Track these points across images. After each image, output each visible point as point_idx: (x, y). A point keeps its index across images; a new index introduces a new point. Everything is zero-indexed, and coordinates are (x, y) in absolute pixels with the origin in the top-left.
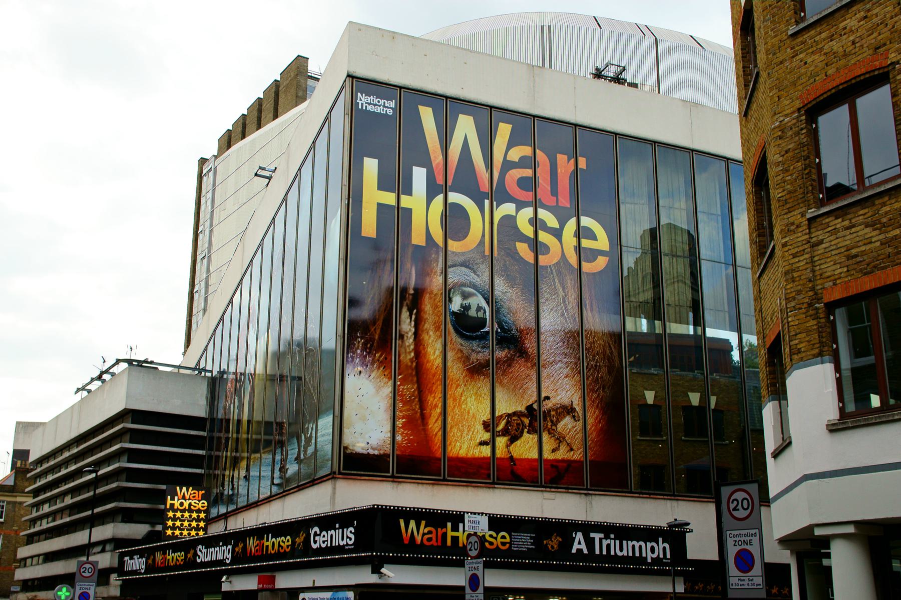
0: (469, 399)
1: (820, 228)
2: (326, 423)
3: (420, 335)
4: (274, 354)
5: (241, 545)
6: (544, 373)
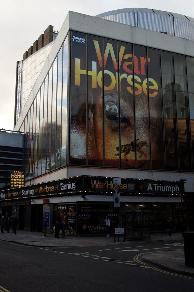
4: (45, 127)
5: (37, 189)
6: (137, 131)
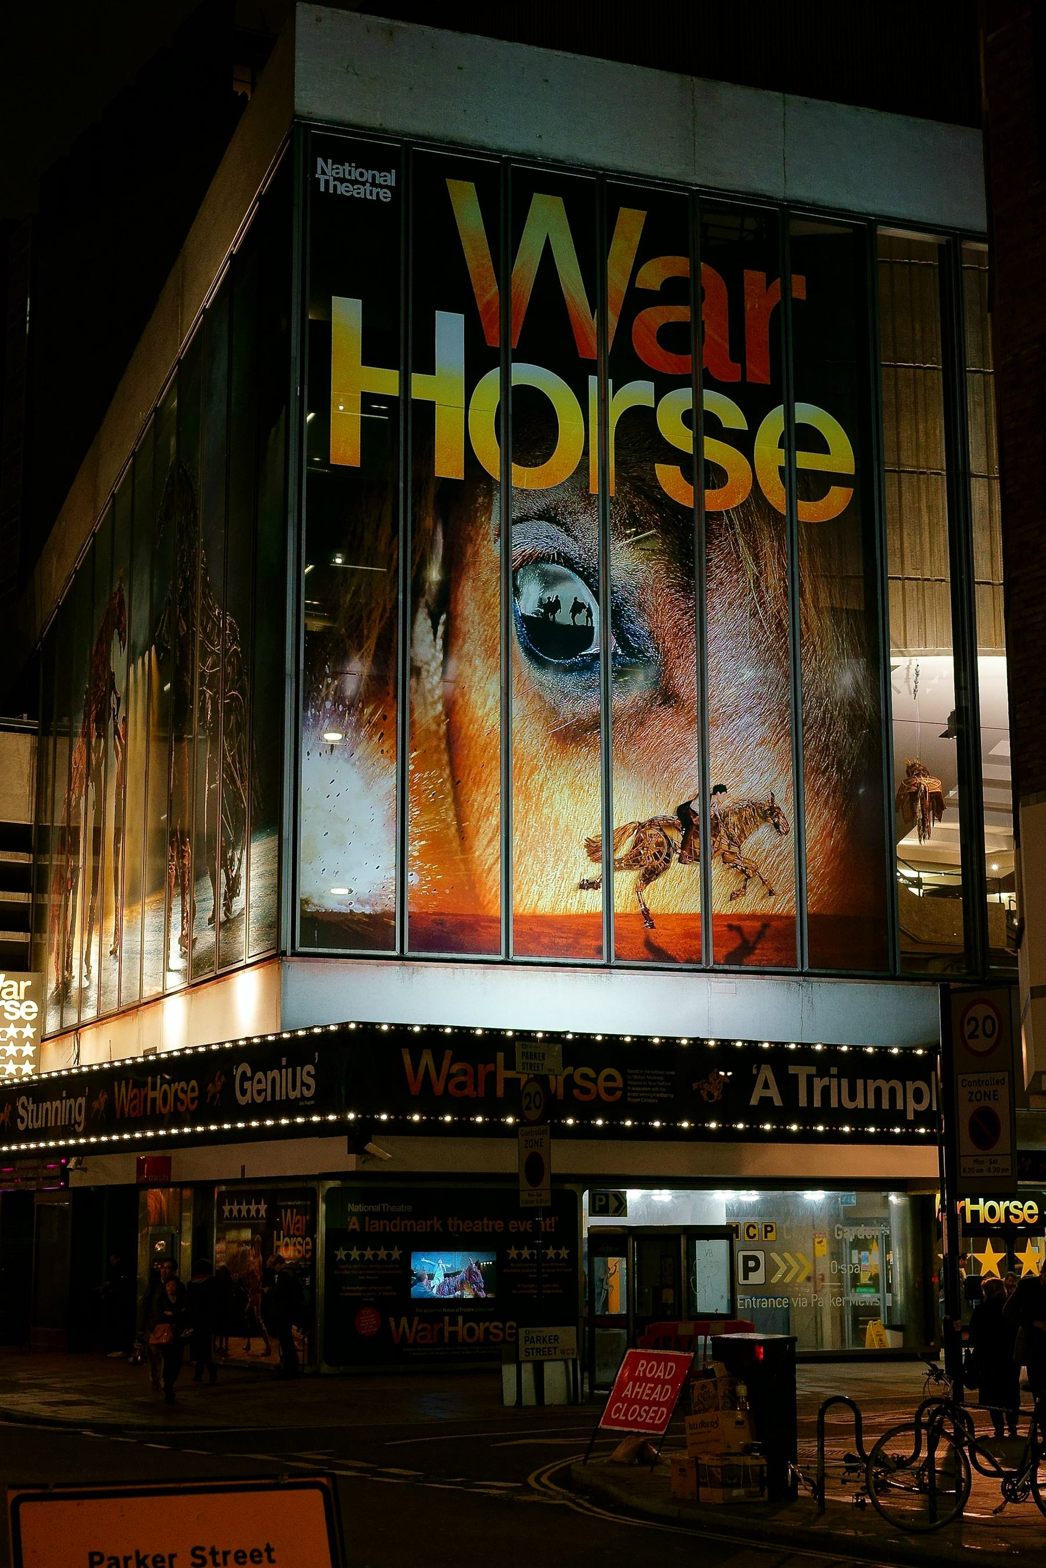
0: (557, 796)
5: (103, 1097)
6: (714, 738)
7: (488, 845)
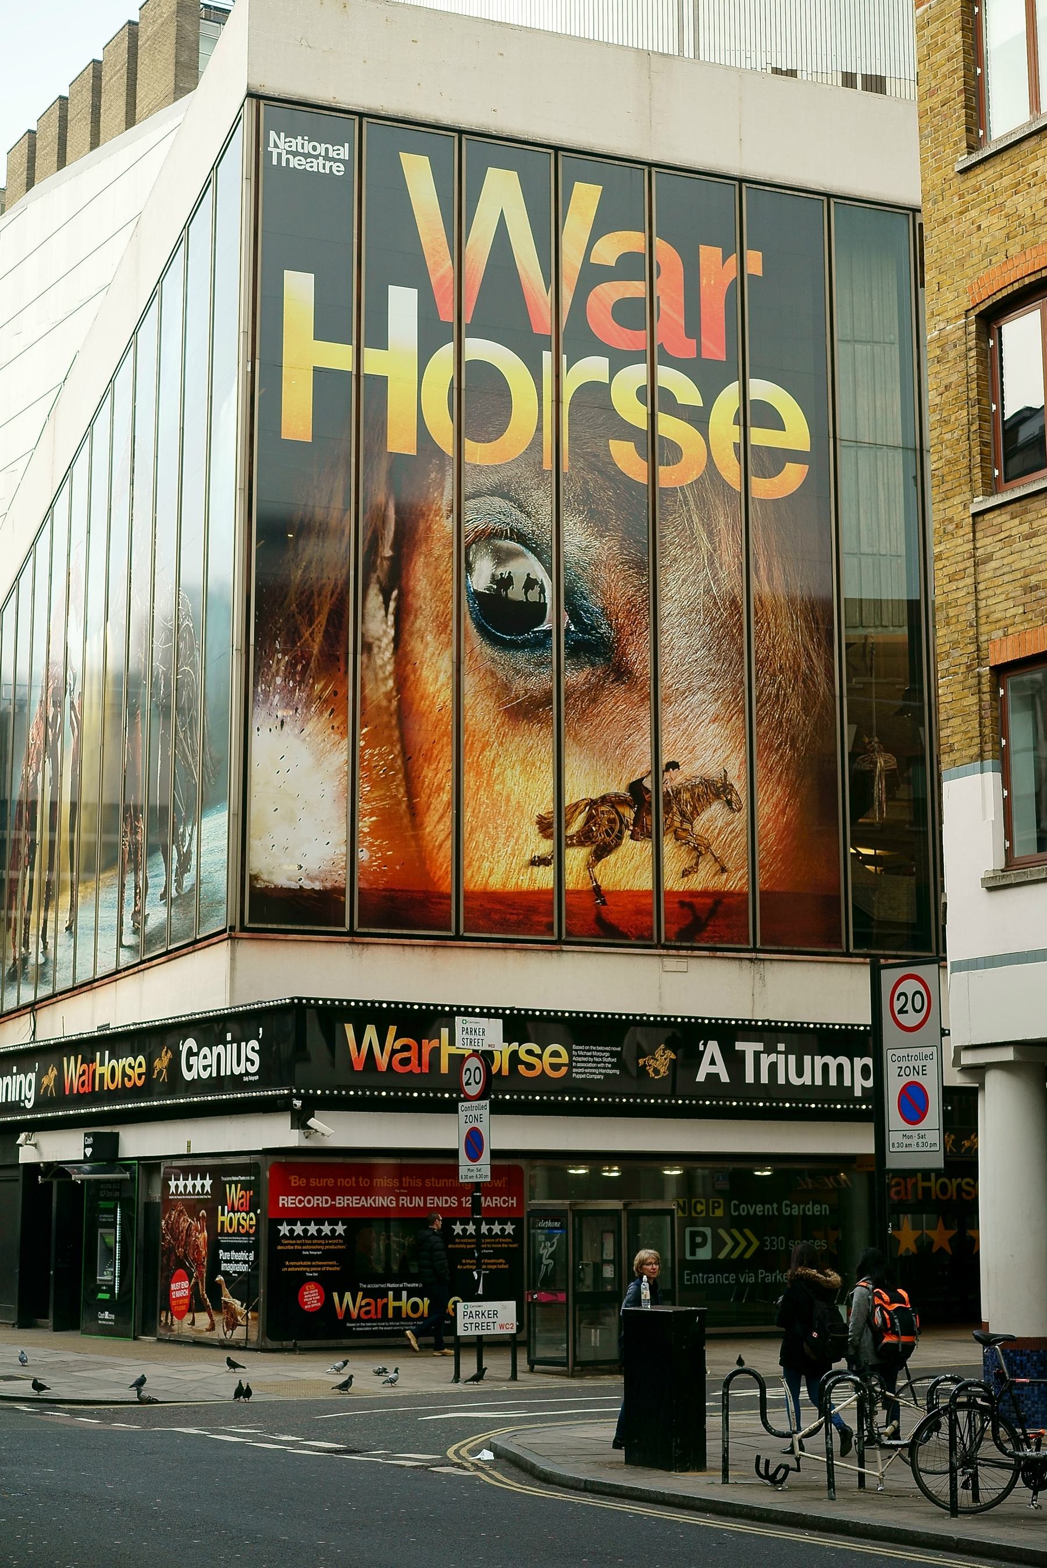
0: (508, 772)
1: (989, 531)
2: (214, 831)
3: (407, 643)
4: (118, 679)
5: (53, 1073)
6: (667, 714)
7: (438, 822)
